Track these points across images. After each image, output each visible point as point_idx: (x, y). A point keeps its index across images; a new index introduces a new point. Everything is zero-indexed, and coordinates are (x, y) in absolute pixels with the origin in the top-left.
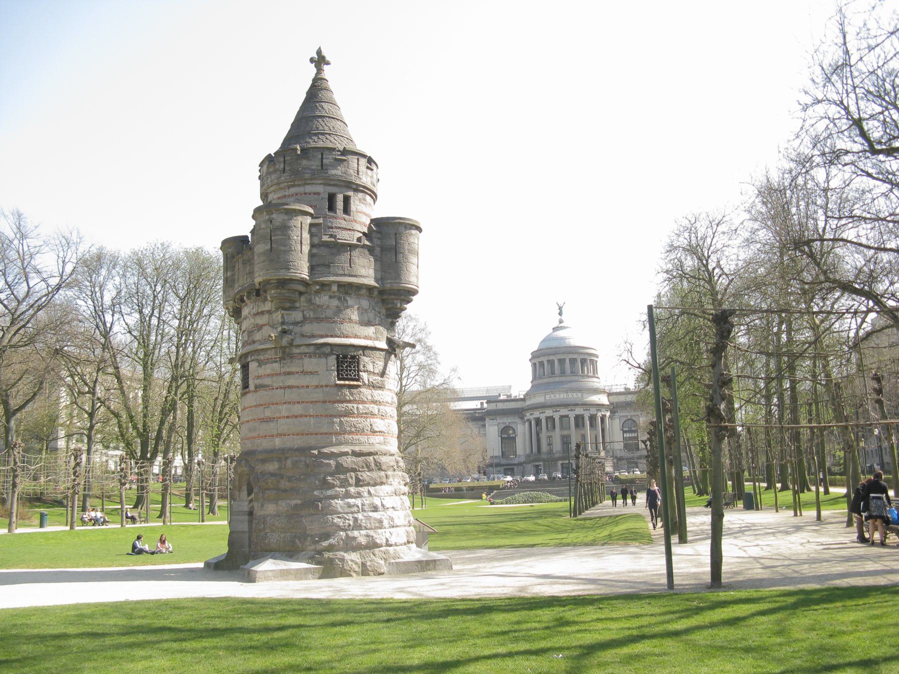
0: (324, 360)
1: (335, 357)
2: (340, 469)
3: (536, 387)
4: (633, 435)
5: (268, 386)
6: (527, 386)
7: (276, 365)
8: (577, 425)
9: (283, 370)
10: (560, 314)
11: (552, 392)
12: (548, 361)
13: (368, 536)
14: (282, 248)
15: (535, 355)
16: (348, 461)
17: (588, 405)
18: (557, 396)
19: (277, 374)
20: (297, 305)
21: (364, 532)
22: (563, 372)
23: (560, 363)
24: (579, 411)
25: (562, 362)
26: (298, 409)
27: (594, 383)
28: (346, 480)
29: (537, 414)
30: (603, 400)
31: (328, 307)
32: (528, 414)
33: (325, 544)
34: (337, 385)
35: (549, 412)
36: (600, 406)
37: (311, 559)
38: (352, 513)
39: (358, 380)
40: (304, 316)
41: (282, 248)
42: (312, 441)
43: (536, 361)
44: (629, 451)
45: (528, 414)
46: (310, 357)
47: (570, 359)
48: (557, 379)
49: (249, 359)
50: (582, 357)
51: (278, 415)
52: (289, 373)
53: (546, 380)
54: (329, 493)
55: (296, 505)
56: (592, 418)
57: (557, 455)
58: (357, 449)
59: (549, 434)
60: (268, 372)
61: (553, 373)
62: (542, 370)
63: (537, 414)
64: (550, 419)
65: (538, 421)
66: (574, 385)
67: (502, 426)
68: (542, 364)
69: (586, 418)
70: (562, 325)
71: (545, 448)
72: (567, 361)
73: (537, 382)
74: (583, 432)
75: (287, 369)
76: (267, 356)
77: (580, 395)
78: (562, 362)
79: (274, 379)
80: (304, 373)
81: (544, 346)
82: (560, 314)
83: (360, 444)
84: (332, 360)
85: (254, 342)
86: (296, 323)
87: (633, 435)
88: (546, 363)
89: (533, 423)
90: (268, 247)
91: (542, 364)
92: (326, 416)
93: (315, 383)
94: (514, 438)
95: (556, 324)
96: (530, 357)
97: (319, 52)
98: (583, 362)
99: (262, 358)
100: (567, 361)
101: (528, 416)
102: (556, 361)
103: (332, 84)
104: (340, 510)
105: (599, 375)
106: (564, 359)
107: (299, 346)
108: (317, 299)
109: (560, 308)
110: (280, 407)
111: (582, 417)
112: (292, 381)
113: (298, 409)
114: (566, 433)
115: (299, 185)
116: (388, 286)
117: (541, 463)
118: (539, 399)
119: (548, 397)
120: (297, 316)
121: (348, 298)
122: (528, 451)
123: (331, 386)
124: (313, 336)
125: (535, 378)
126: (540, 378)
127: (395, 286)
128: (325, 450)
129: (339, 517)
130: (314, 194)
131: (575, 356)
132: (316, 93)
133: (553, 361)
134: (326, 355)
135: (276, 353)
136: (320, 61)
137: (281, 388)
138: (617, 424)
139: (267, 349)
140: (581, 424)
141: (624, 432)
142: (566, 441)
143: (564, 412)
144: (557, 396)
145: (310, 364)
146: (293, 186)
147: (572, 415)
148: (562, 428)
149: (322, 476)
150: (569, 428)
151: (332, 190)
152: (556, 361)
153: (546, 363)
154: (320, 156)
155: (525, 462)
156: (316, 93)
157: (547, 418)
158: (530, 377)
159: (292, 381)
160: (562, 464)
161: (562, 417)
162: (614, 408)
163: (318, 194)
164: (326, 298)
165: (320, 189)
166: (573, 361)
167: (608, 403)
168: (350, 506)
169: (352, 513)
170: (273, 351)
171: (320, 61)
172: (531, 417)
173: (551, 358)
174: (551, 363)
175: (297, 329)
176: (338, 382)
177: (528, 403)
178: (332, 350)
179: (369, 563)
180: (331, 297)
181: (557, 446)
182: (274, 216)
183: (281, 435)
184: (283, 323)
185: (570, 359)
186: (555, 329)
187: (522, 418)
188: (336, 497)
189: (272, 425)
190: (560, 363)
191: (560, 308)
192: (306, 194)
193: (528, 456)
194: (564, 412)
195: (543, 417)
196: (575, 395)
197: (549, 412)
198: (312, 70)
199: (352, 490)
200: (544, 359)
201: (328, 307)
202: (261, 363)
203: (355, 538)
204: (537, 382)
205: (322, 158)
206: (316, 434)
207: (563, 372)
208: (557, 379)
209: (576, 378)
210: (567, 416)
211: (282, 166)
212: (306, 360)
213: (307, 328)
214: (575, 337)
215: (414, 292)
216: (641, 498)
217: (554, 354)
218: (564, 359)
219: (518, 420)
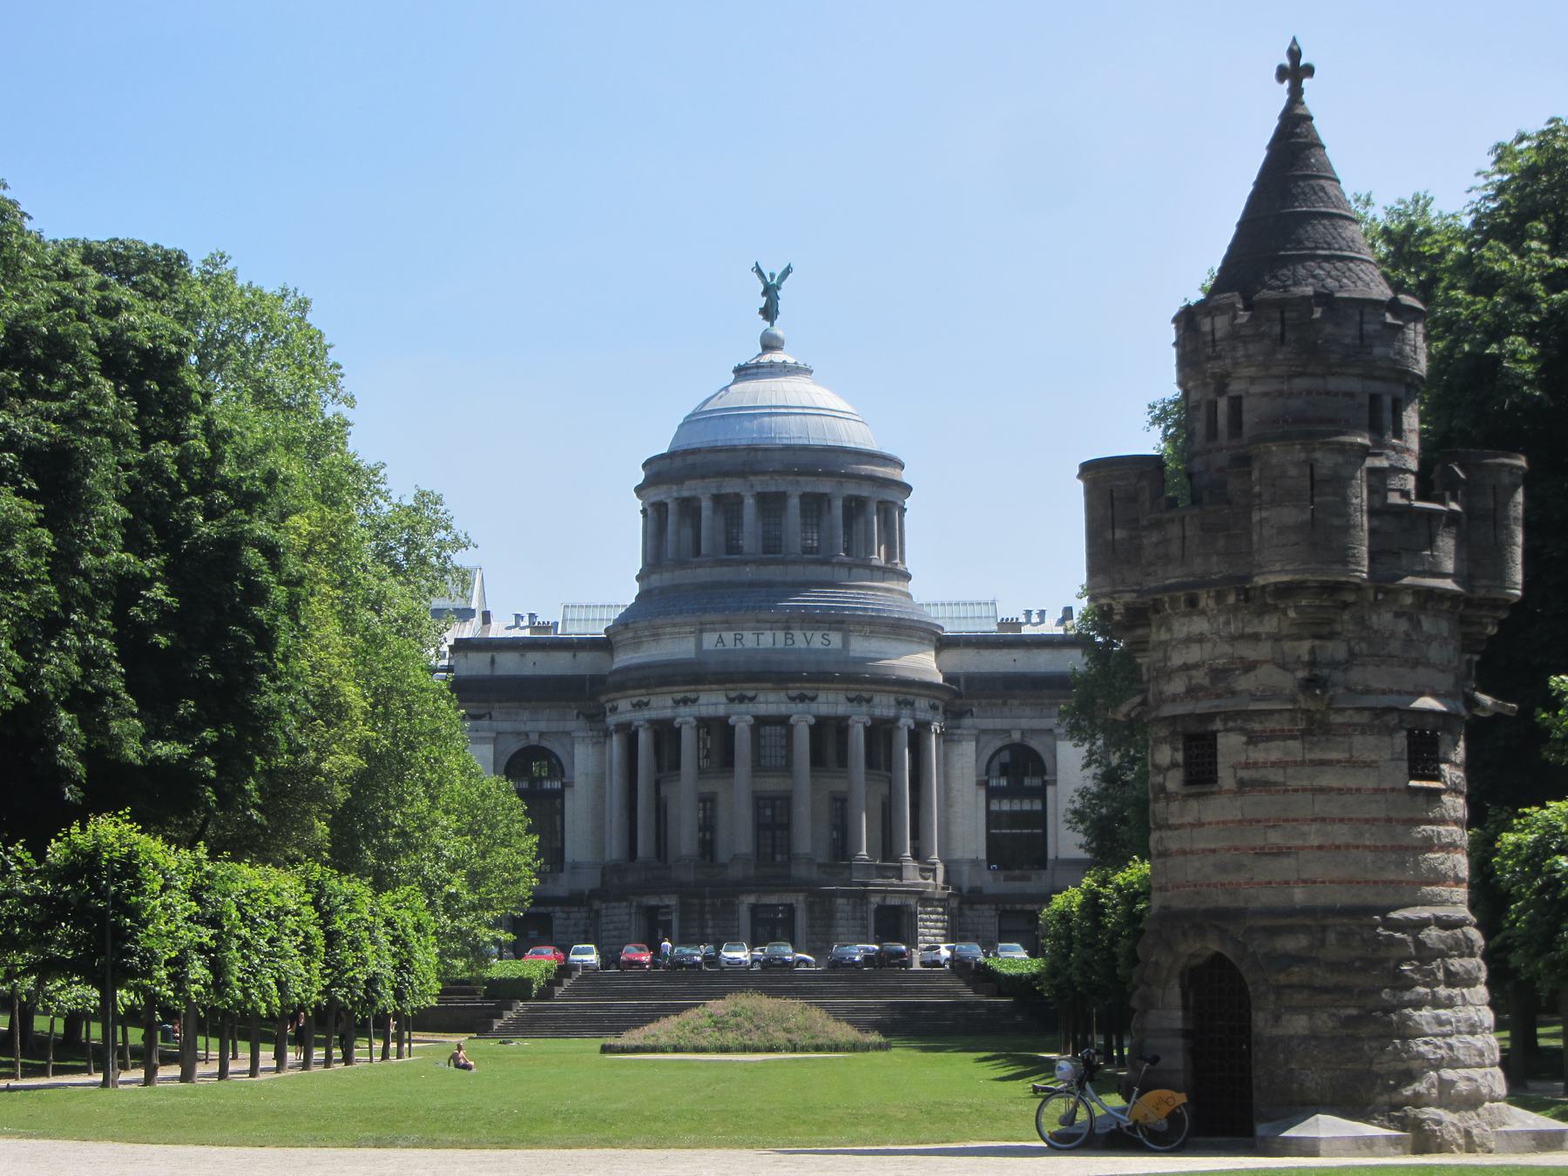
0: (1387, 739)
1: (1405, 733)
2: (1425, 954)
3: (657, 601)
4: (1026, 806)
5: (1275, 784)
6: (627, 592)
7: (1294, 745)
8: (817, 760)
9: (1309, 756)
10: (769, 312)
11: (728, 625)
12: (717, 499)
13: (1469, 1079)
14: (1336, 522)
15: (661, 473)
16: (1432, 935)
17: (863, 681)
18: (749, 640)
19: (1295, 763)
20: (1338, 628)
21: (1462, 1072)
22: (772, 547)
23: (761, 515)
24: (830, 703)
25: (771, 504)
26: (1341, 834)
27: (876, 596)
28: (1432, 973)
29: (662, 706)
30: (924, 664)
31: (1393, 635)
32: (624, 705)
33: (1408, 1091)
34: (1410, 788)
35: (712, 703)
36: (908, 688)
37: (1393, 1122)
38: (1444, 1035)
39: (1436, 778)
40: (1352, 654)
41: (1336, 522)
42: (1369, 897)
43: (667, 494)
44: (1004, 866)
45: (624, 705)
46: (1363, 733)
47: (804, 497)
48: (749, 573)
49: (1218, 725)
50: (851, 489)
51: (1299, 843)
52: (1323, 763)
53: (704, 574)
54: (1407, 996)
55: (1349, 1018)
56: (881, 733)
57: (736, 872)
58: (1441, 911)
59: (709, 786)
60: (1274, 756)
61: (732, 547)
62: (687, 532)
63: (662, 706)
64: (718, 731)
65: (666, 733)
66: (813, 599)
67: (514, 746)
68: (689, 507)
69: (869, 739)
70: (777, 357)
71: (685, 839)
72: (794, 503)
73: (656, 580)
74: (839, 785)
75: (1317, 755)
76: (1271, 725)
77: (836, 639)
78: (771, 504)
79: (1290, 771)
80: (1352, 764)
81: (700, 439)
82: (769, 312)
83: (1442, 903)
84: (1401, 740)
85: (1234, 693)
86: (1334, 664)
87: (1026, 806)
88: (706, 505)
89: (644, 738)
90: (1307, 516)
91: (689, 507)
92: (1393, 849)
93: (1371, 784)
94: (560, 794)
95: (750, 352)
96: (640, 476)
97: (1294, 54)
98: (855, 508)
99: (1257, 727)
100: (794, 503)
101: (624, 710)
102: (749, 502)
103: (1325, 126)
104: (1427, 1029)
105: (910, 564)
106: (781, 497)
107: (1343, 710)
108: (1374, 617)
109: (770, 291)
110: (1305, 828)
111: (840, 726)
112: (1328, 779)
113: (1341, 834)
114: (772, 784)
115: (1312, 375)
116: (1482, 593)
117: (671, 901)
118: (676, 647)
119: (710, 641)
120: (1336, 650)
121: (1422, 617)
122: (615, 851)
123: (1400, 790)
124: (1368, 691)
125: (655, 558)
126: (681, 563)
127: (1495, 594)
128: (1394, 915)
129: (1426, 1043)
130: (1346, 394)
131: (824, 486)
132: (1293, 152)
133: (738, 499)
134: (1391, 731)
135: (1293, 720)
136: (1295, 72)
137: (1305, 790)
138: (967, 758)
139: (1272, 712)
140: (831, 752)
141: (992, 793)
142: (773, 819)
143: (771, 703)
144: (749, 640)
145: (1366, 746)
146: (1300, 375)
147: (803, 719)
148: (758, 767)
149: (1392, 964)
150: (787, 768)
151: (1377, 387)
152: (749, 502)
153: (706, 505)
154: (1358, 318)
155: (593, 894)
156: (1293, 152)
157: (704, 723)
158: (635, 562)
159: (1328, 779)
160: (754, 909)
161: (761, 722)
162: (960, 697)
163: (1352, 395)
164: (1388, 616)
165: (1353, 385)
166: (815, 505)
167: (939, 679)
168: (1440, 1023)
169: (1444, 1035)
170: (1287, 715)
171: (1295, 72)
172: (639, 717)
173: (731, 486)
174: (728, 506)
175: (1338, 676)
176: (1413, 783)
177: (623, 659)
178: (1401, 721)
179: (1475, 1131)
180: (1397, 615)
181: (737, 835)
182: (1318, 455)
183: (1305, 882)
184: (1312, 664)
185: (804, 497)
186: (743, 372)
187: (595, 717)
188: (1418, 1005)
189: (1287, 862)
190: (761, 515)
191: (770, 291)
192: (1328, 393)
193: (608, 870)
194: (771, 703)
195: (685, 716)
196: (817, 641)
197: (712, 703)
198: (1282, 91)
199: (1442, 991)
200: (703, 491)
201: (1393, 635)
202: (1253, 739)
203: (1452, 1083)
204: (656, 580)
205: (1362, 323)
206: (1376, 882)
207: (772, 547)
208: (749, 573)
209: (822, 572)
210: (783, 721)
211: (1277, 329)
212: (1358, 740)
213: (1357, 676)
214: (823, 404)
215: (1094, 472)
216: (266, 1059)
217: (741, 474)
218: (781, 497)
219: (574, 725)
